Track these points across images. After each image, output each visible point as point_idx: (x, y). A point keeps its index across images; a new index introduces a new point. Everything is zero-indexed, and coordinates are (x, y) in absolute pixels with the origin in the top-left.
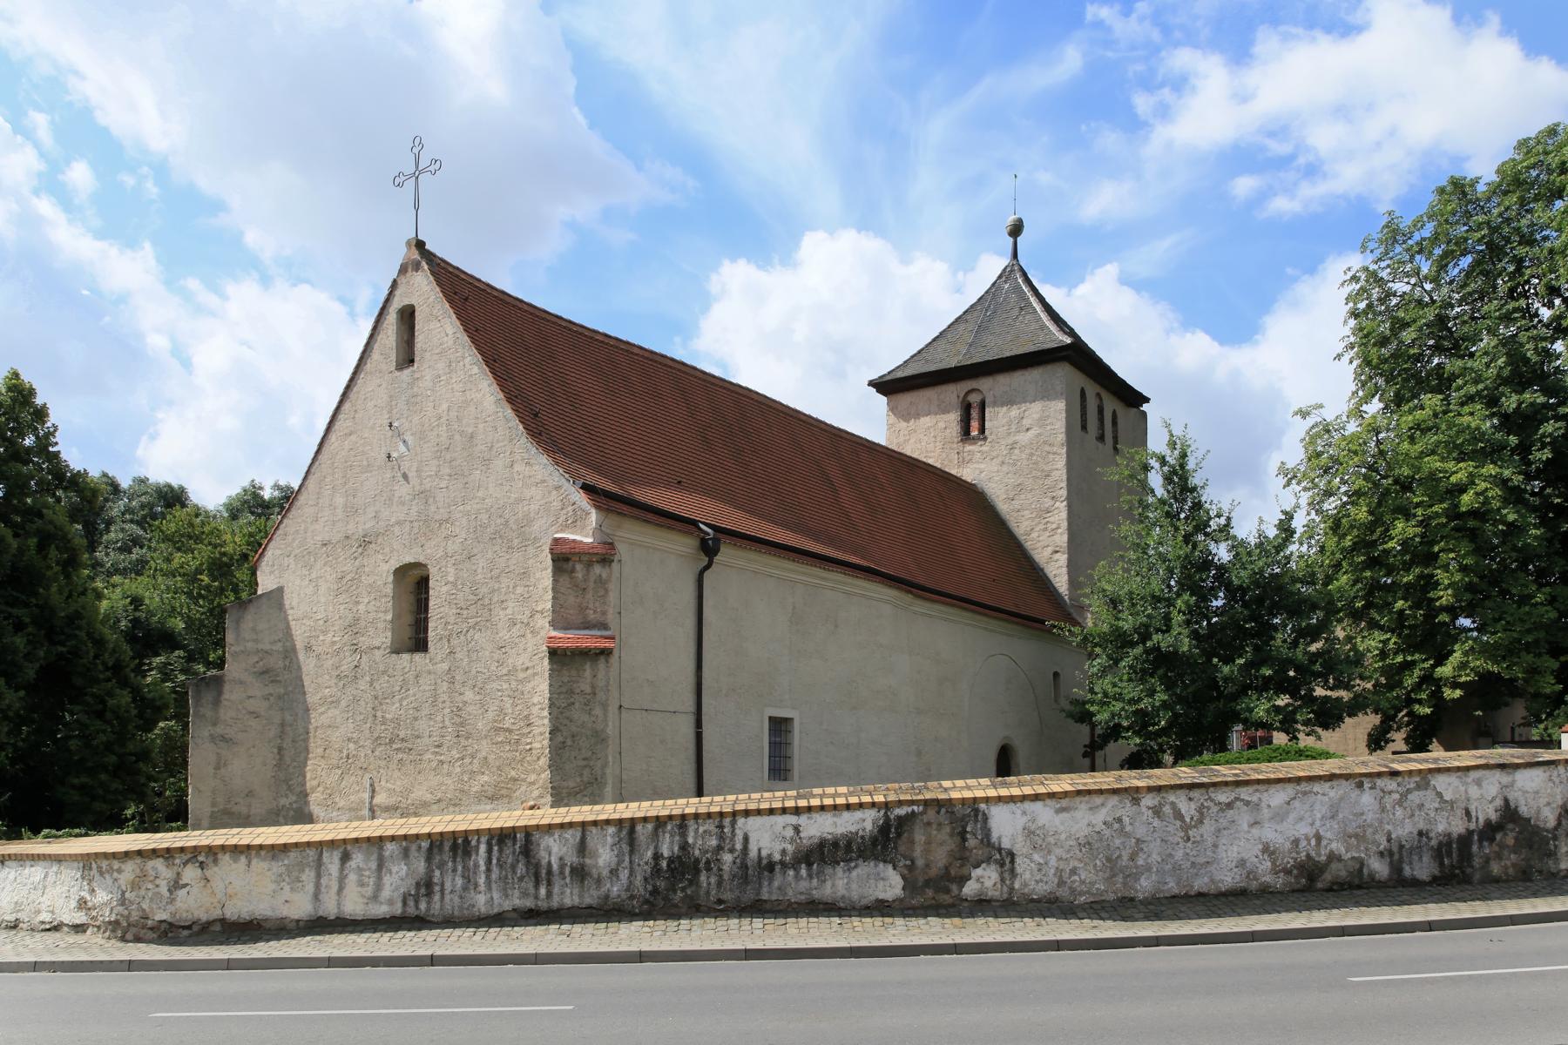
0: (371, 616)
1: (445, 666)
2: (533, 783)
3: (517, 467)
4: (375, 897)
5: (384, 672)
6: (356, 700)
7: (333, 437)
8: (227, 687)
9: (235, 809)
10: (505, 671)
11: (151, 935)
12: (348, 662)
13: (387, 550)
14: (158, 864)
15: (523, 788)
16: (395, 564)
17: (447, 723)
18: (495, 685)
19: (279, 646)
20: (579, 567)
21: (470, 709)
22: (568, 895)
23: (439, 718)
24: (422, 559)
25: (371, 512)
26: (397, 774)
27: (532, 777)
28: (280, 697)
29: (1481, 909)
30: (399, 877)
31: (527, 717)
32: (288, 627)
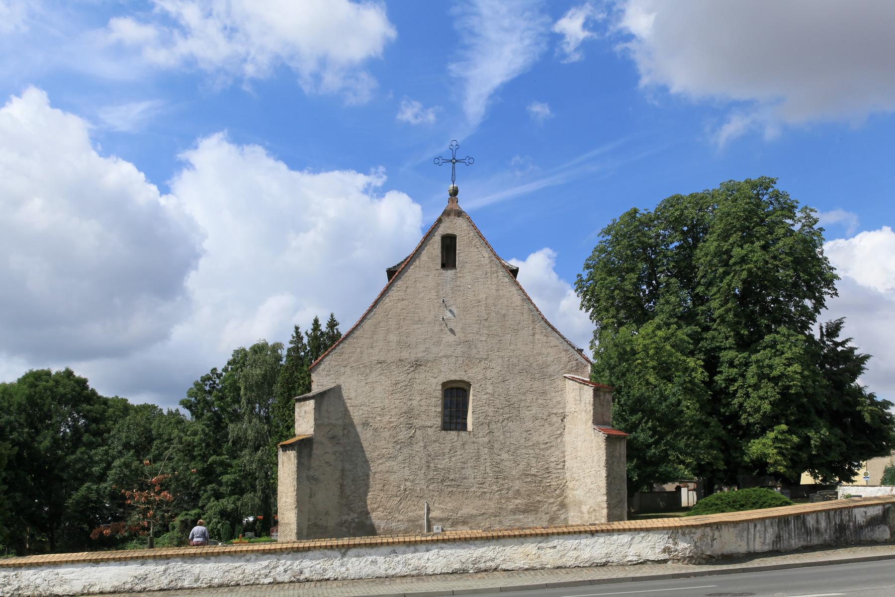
0: (423, 409)
1: (486, 439)
2: (553, 503)
3: (537, 336)
4: (764, 543)
5: (435, 441)
6: (411, 456)
7: (386, 300)
8: (315, 446)
9: (320, 523)
10: (531, 444)
11: (704, 562)
12: (403, 435)
13: (435, 371)
14: (708, 529)
15: (546, 506)
16: (443, 378)
17: (488, 470)
18: (524, 451)
19: (340, 422)
20: (602, 394)
21: (507, 463)
22: (815, 541)
23: (482, 468)
24: (465, 379)
25: (422, 347)
26: (448, 499)
27: (552, 500)
28: (341, 454)
29: (738, 566)
30: (771, 534)
31: (547, 468)
32: (346, 411)
